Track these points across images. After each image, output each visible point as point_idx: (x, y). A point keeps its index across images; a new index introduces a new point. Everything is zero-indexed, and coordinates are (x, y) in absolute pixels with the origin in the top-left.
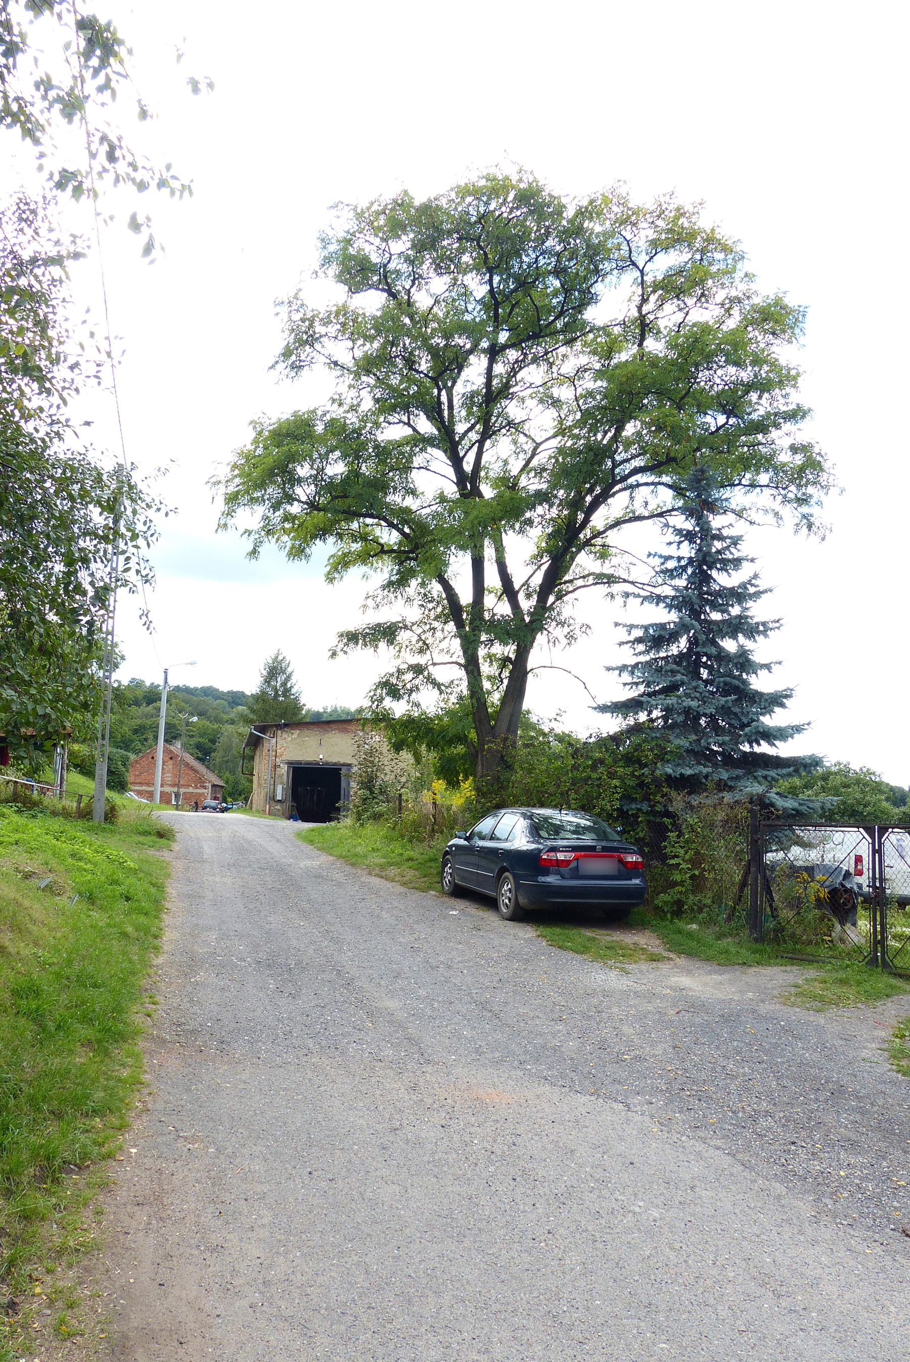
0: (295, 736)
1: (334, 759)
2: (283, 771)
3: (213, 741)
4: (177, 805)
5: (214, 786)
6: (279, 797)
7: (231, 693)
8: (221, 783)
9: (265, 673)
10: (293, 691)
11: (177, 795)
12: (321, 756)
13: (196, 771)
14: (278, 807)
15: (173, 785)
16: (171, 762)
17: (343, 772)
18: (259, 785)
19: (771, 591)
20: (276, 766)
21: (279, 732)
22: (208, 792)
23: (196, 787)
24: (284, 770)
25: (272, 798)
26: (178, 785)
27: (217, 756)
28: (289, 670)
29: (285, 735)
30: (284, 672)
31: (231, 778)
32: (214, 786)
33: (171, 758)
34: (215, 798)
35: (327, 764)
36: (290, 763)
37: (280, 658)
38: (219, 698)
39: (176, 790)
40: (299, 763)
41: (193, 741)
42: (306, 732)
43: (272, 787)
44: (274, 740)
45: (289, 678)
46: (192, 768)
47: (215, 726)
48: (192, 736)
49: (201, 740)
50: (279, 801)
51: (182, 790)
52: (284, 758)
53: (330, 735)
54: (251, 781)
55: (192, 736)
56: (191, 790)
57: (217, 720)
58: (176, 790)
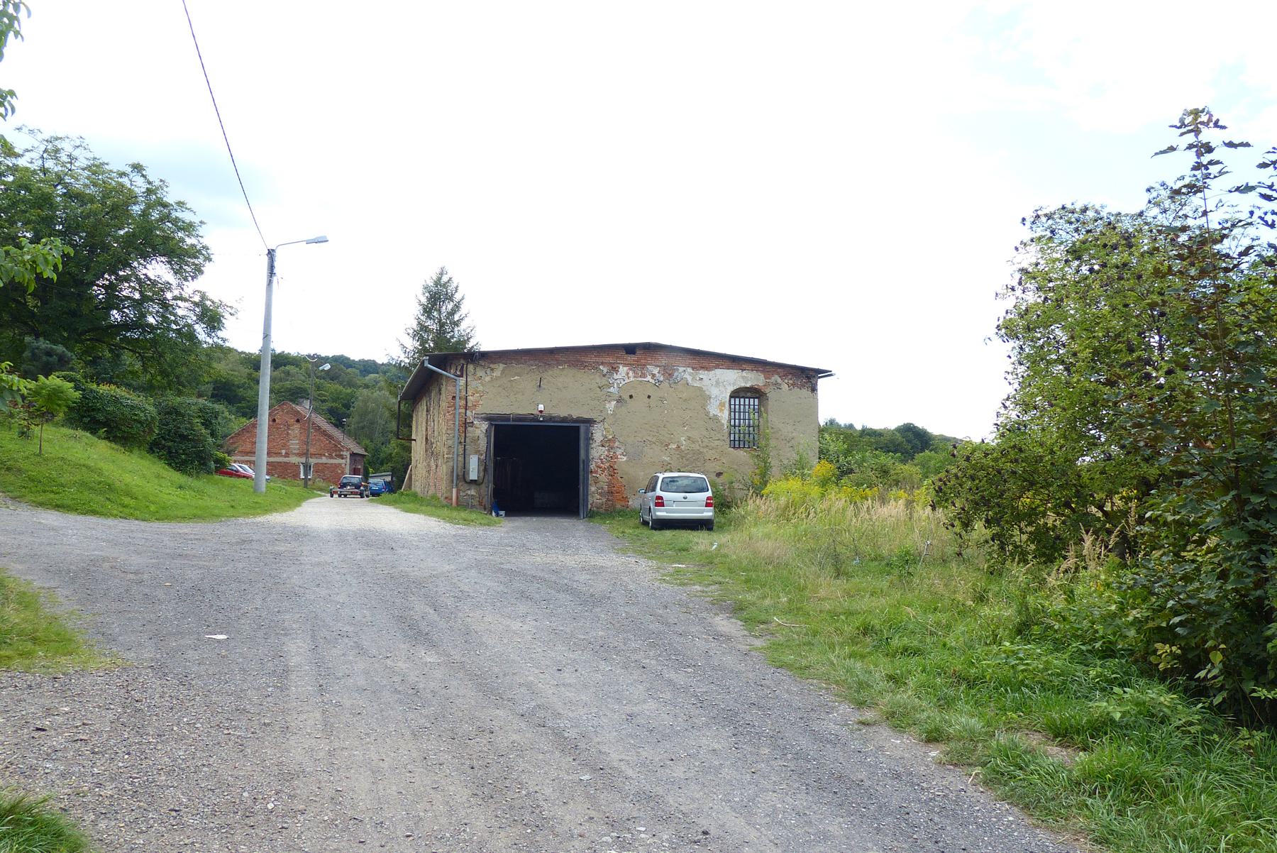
0: (497, 373)
1: (562, 411)
2: (478, 432)
3: (347, 406)
4: (306, 480)
5: (353, 455)
6: (473, 475)
7: (362, 362)
8: (362, 452)
9: (424, 300)
10: (463, 325)
11: (307, 467)
12: (541, 407)
13: (330, 437)
14: (472, 492)
15: (300, 455)
16: (298, 426)
17: (583, 428)
18: (430, 451)
19: (1247, 145)
20: (466, 424)
21: (471, 367)
22: (346, 463)
23: (331, 457)
24: (480, 429)
25: (461, 477)
26: (305, 454)
27: (352, 422)
28: (457, 297)
29: (480, 373)
30: (451, 298)
31: (371, 446)
32: (353, 455)
33: (298, 421)
34: (355, 472)
35: (551, 419)
36: (489, 418)
37: (445, 279)
38: (351, 366)
39: (303, 460)
40: (505, 418)
41: (325, 406)
42: (517, 367)
43: (461, 459)
44: (462, 381)
45: (457, 307)
46: (325, 433)
47: (349, 391)
48: (323, 401)
49: (334, 405)
50: (473, 482)
51: (312, 461)
52: (479, 410)
53: (556, 371)
54: (409, 450)
55: (323, 401)
56: (324, 460)
57: (351, 384)
58: (303, 460)
